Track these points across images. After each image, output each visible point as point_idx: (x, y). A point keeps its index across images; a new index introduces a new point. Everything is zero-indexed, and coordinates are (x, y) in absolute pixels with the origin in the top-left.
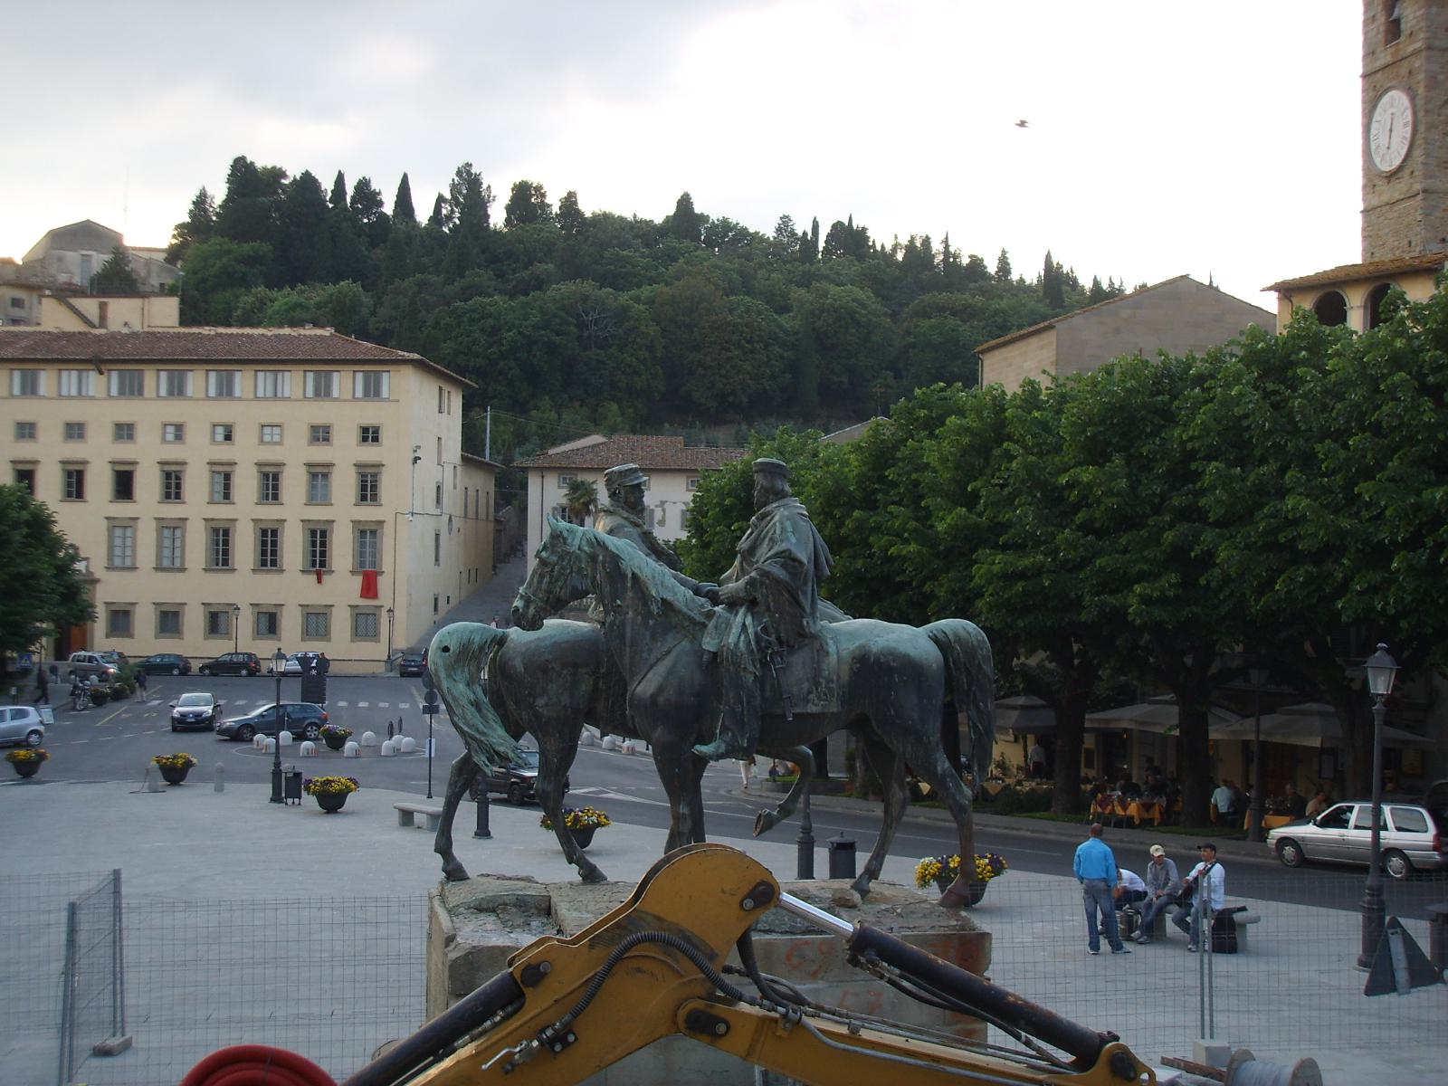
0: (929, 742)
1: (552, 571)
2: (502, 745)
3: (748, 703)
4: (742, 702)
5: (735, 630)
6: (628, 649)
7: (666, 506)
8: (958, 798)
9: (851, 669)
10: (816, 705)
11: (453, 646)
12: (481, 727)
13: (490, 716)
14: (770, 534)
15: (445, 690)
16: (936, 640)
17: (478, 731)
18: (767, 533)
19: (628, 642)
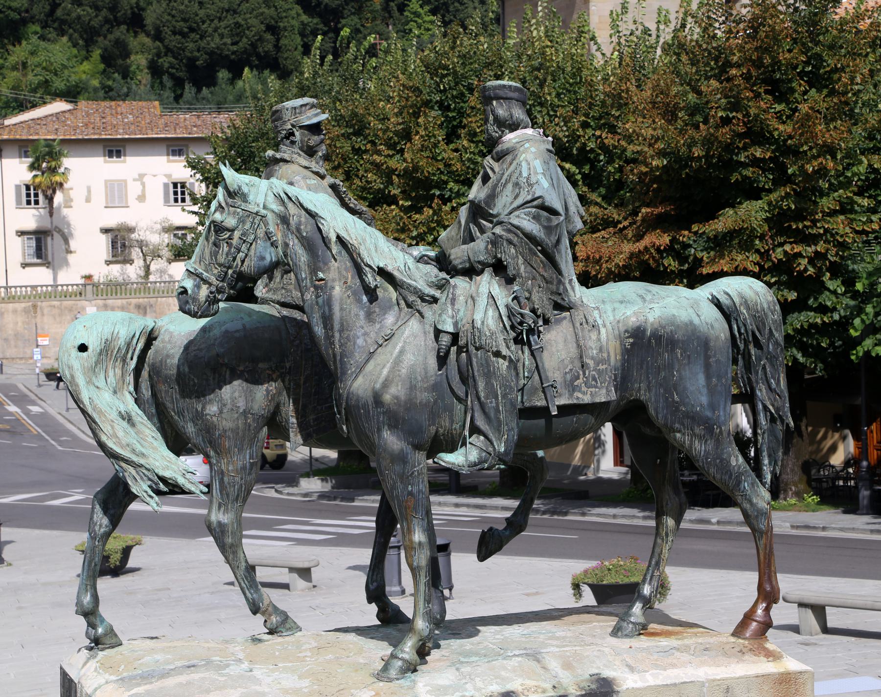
0: (721, 432)
1: (230, 238)
2: (167, 468)
3: (504, 396)
4: (496, 398)
5: (482, 301)
6: (337, 335)
7: (145, 180)
8: (755, 501)
9: (622, 344)
10: (584, 393)
11: (94, 345)
12: (138, 448)
13: (147, 432)
14: (514, 179)
15: (86, 401)
16: (718, 304)
17: (133, 451)
18: (510, 176)
19: (337, 326)
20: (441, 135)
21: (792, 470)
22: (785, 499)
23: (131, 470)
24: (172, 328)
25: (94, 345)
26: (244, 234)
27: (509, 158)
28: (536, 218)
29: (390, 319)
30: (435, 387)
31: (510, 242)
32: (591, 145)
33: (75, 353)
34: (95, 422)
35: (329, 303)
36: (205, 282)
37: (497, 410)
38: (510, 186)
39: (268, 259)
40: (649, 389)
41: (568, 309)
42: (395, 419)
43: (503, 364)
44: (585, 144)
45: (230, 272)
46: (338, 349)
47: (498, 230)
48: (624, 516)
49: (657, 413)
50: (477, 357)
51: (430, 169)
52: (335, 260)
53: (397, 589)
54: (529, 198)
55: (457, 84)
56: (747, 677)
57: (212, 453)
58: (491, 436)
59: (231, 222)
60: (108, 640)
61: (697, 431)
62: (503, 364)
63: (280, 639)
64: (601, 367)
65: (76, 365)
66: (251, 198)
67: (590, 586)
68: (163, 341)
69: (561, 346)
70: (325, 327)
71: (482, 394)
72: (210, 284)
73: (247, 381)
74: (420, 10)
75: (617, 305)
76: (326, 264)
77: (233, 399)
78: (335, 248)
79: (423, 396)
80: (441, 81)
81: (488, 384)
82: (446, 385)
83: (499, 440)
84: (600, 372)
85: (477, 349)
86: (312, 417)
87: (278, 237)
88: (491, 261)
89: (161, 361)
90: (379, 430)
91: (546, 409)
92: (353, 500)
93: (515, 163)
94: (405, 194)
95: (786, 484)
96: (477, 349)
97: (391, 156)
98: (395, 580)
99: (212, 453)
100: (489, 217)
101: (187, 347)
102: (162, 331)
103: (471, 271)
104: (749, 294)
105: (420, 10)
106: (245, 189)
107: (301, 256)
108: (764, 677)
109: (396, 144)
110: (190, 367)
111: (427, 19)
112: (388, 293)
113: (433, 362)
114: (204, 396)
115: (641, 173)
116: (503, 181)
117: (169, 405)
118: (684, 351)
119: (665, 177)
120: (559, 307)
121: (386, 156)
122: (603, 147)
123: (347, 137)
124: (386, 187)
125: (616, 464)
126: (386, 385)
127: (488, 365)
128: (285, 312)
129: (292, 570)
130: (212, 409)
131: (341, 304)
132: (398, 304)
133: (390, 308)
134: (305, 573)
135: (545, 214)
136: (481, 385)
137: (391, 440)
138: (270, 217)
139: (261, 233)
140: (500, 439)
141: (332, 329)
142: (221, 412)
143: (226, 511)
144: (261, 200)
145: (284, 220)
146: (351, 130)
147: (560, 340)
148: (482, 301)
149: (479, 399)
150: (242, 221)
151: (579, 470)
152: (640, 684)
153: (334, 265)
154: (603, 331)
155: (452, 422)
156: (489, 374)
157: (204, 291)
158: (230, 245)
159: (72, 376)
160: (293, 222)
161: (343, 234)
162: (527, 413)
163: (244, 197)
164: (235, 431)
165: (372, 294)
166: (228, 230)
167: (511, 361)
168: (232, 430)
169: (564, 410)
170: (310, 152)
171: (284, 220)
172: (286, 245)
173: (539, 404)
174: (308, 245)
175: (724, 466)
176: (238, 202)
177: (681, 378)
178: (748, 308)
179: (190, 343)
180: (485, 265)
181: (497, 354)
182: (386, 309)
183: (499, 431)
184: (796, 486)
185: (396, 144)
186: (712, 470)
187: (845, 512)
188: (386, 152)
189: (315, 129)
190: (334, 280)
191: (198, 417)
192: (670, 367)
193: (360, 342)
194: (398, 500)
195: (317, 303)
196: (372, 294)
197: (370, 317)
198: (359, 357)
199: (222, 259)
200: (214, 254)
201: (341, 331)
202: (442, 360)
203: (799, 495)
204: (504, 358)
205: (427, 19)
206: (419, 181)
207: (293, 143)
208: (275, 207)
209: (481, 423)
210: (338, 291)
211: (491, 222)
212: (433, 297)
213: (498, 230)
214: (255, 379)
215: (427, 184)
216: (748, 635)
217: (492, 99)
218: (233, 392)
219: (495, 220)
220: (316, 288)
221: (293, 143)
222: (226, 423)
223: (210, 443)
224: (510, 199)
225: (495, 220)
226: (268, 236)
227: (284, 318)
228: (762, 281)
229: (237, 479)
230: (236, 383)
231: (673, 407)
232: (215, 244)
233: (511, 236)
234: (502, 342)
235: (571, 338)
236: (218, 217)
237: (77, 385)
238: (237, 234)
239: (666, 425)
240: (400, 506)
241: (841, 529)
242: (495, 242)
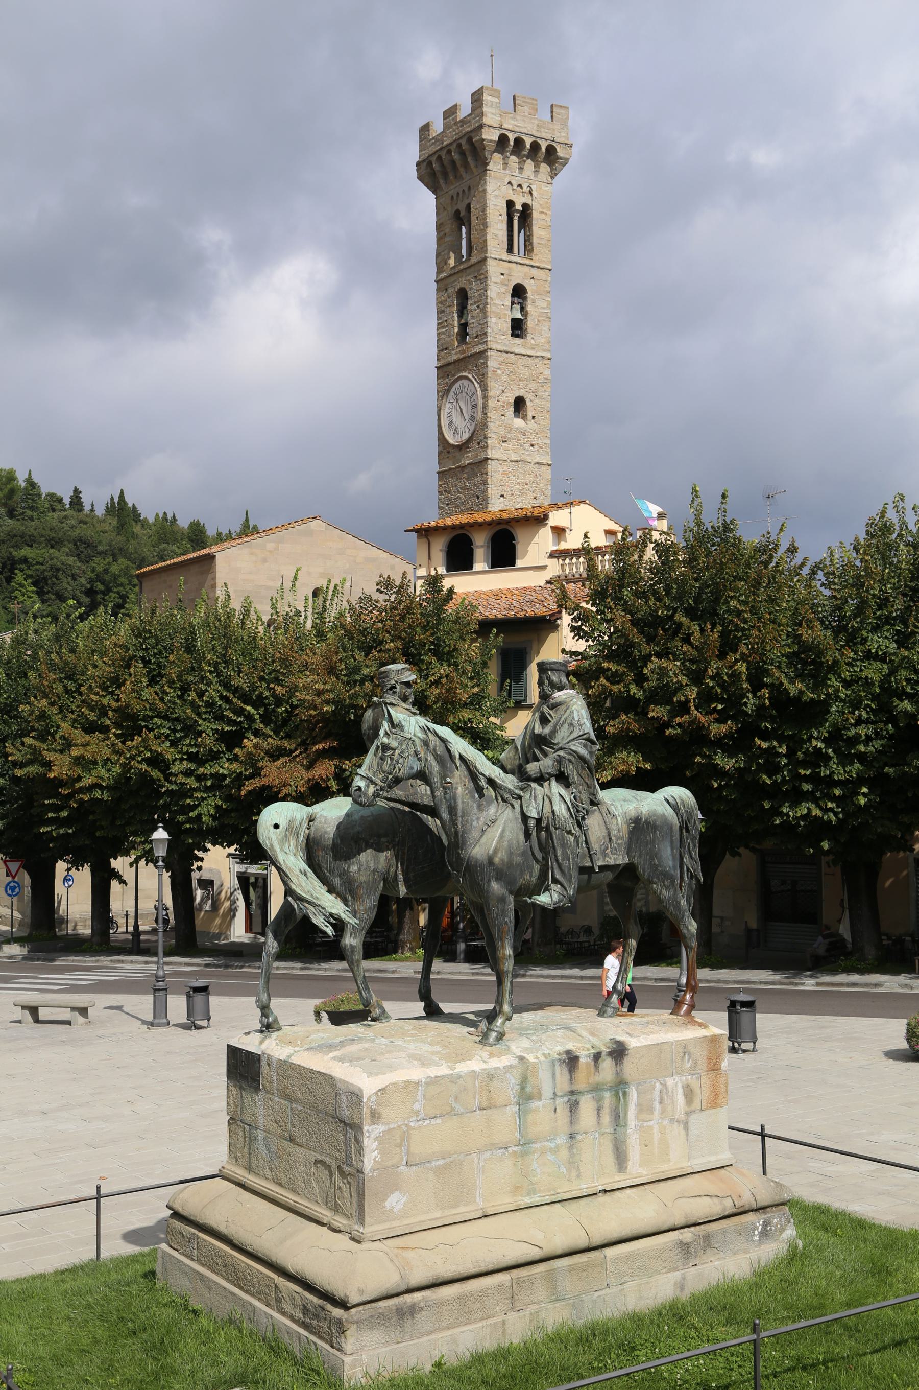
2: (333, 907)
3: (573, 859)
6: (460, 819)
11: (283, 824)
12: (315, 894)
14: (569, 721)
17: (312, 895)
19: (459, 813)
20: (145, 681)
21: (408, 932)
22: (403, 953)
23: (312, 908)
24: (325, 814)
25: (283, 824)
26: (402, 752)
27: (563, 707)
28: (585, 746)
29: (492, 810)
30: (524, 854)
31: (570, 761)
32: (267, 694)
33: (272, 829)
34: (287, 876)
35: (454, 798)
36: (372, 782)
37: (569, 868)
38: (566, 726)
39: (415, 769)
40: (640, 856)
41: (597, 805)
42: (500, 875)
43: (572, 838)
44: (262, 693)
45: (390, 777)
46: (460, 828)
47: (562, 753)
48: (285, 968)
49: (644, 871)
50: (556, 834)
51: (138, 707)
52: (457, 768)
53: (165, 1021)
54: (581, 733)
55: (157, 644)
56: (694, 1038)
57: (350, 898)
58: (565, 885)
59: (394, 744)
60: (275, 1026)
61: (666, 883)
62: (572, 838)
63: (381, 1025)
64: (619, 842)
65: (274, 838)
66: (406, 729)
67: (326, 1012)
68: (320, 822)
69: (597, 828)
70: (450, 813)
71: (560, 858)
72: (376, 784)
73: (375, 849)
74: (24, 582)
75: (622, 803)
76: (452, 773)
77: (367, 862)
78: (458, 763)
79: (518, 859)
80: (144, 642)
81: (564, 851)
82: (530, 852)
83: (570, 887)
84: (619, 845)
85: (556, 829)
86: (412, 874)
87: (422, 755)
88: (555, 773)
89: (321, 836)
90: (489, 881)
91: (592, 868)
92: (53, 960)
93: (568, 711)
94: (118, 725)
95: (404, 942)
96: (556, 829)
97: (104, 696)
98: (163, 1015)
99: (350, 898)
100: (551, 745)
101: (338, 827)
102: (318, 816)
103: (541, 779)
104: (684, 797)
105: (24, 582)
106: (403, 723)
107: (435, 768)
108: (703, 1038)
109: (107, 687)
110: (341, 840)
111: (30, 589)
112: (490, 792)
113: (522, 837)
114: (349, 859)
115: (311, 715)
116: (561, 722)
117: (324, 865)
118: (661, 832)
119: (332, 719)
120: (593, 803)
121: (100, 696)
122: (274, 695)
123: (60, 680)
124: (99, 719)
125: (246, 932)
126: (496, 851)
127: (563, 839)
128: (392, 804)
129: (73, 1009)
130: (354, 868)
131: (463, 799)
132: (497, 799)
133: (492, 802)
134: (83, 1011)
135: (589, 744)
136: (559, 852)
137: (496, 887)
138: (417, 741)
139: (412, 751)
140: (570, 887)
141: (456, 814)
142: (359, 870)
143: (355, 938)
144: (412, 730)
145: (426, 743)
146: (63, 676)
147: (596, 824)
148: (556, 799)
149: (557, 861)
150: (401, 743)
151: (218, 936)
152: (639, 1045)
153: (457, 773)
154: (619, 819)
155: (531, 876)
156: (564, 845)
157: (372, 789)
158: (392, 759)
159: (272, 845)
160: (432, 744)
161: (463, 753)
162: (583, 870)
163: (402, 728)
164: (367, 883)
165: (480, 790)
166: (392, 749)
167: (576, 837)
168: (366, 883)
169: (602, 868)
170: (405, 699)
171: (426, 743)
172: (426, 760)
173: (587, 865)
174: (440, 760)
175: (678, 906)
176: (398, 730)
177: (659, 849)
178: (684, 806)
179: (340, 823)
180: (551, 775)
181: (569, 832)
182: (489, 803)
183: (570, 882)
184: (410, 943)
185: (107, 687)
186: (671, 908)
187: (445, 962)
188: (101, 693)
189: (408, 684)
190: (457, 783)
191: (344, 874)
192: (653, 842)
193: (475, 823)
194: (499, 927)
195: (445, 798)
196: (480, 790)
197: (479, 807)
198: (475, 834)
199: (386, 768)
200: (380, 765)
201: (462, 817)
202: (527, 835)
203: (412, 950)
204: (572, 834)
205: (30, 589)
206: (129, 714)
207: (395, 693)
208: (421, 735)
209: (558, 876)
210: (460, 790)
211: (553, 748)
212: (518, 795)
213: (562, 753)
214: (379, 849)
215: (134, 717)
216: (682, 1013)
217: (548, 670)
218: (366, 857)
219: (555, 747)
220: (444, 788)
221: (395, 693)
222: (362, 878)
223: (350, 891)
224: (566, 734)
225: (555, 747)
226: (416, 753)
227: (392, 808)
228: (284, 799)
229: (365, 916)
230: (369, 851)
231: (654, 868)
232: (381, 758)
233: (570, 757)
234: (571, 825)
235: (602, 822)
236: (385, 740)
237: (275, 851)
238: (397, 752)
239: (649, 879)
240: (499, 931)
241: (451, 973)
242: (560, 760)
